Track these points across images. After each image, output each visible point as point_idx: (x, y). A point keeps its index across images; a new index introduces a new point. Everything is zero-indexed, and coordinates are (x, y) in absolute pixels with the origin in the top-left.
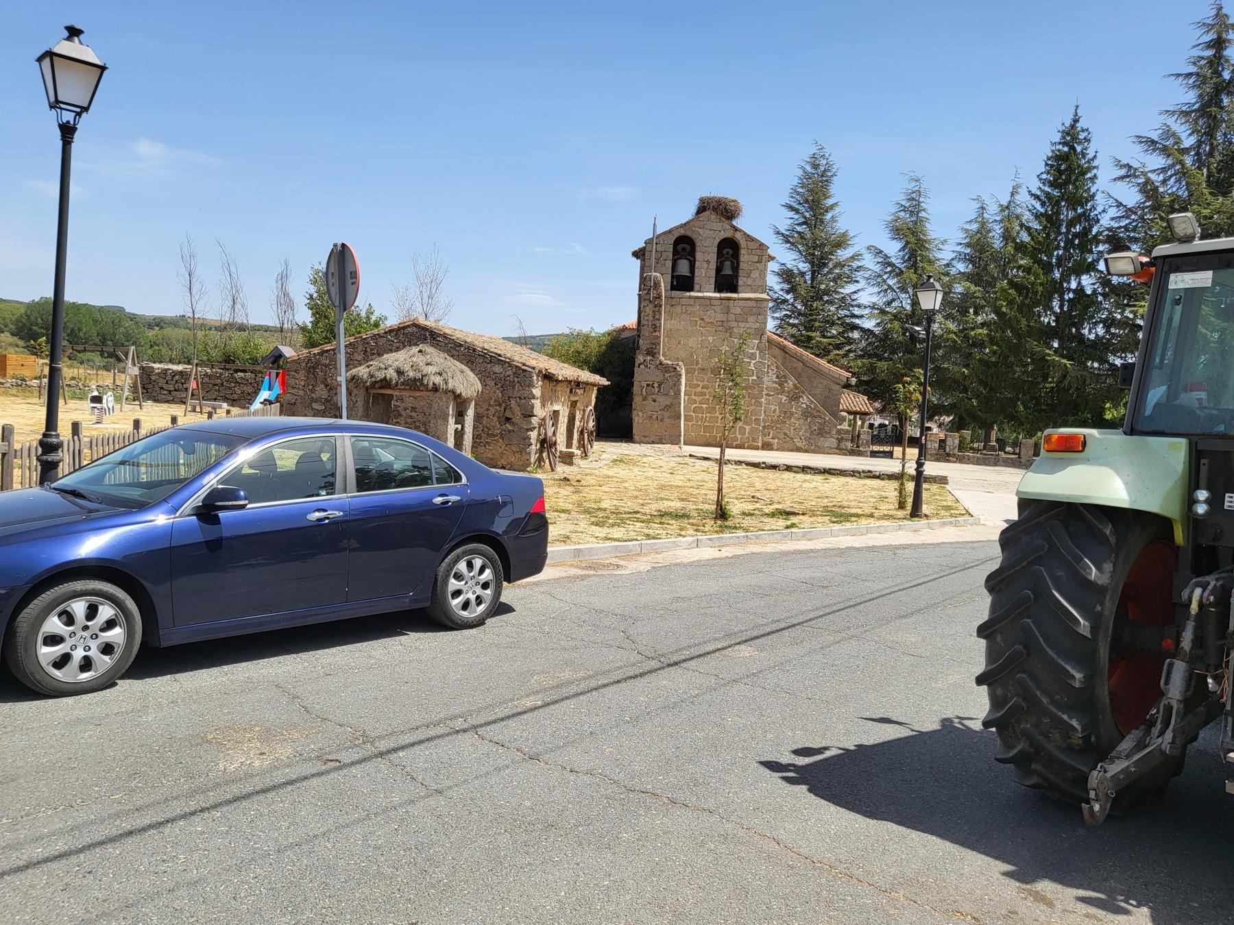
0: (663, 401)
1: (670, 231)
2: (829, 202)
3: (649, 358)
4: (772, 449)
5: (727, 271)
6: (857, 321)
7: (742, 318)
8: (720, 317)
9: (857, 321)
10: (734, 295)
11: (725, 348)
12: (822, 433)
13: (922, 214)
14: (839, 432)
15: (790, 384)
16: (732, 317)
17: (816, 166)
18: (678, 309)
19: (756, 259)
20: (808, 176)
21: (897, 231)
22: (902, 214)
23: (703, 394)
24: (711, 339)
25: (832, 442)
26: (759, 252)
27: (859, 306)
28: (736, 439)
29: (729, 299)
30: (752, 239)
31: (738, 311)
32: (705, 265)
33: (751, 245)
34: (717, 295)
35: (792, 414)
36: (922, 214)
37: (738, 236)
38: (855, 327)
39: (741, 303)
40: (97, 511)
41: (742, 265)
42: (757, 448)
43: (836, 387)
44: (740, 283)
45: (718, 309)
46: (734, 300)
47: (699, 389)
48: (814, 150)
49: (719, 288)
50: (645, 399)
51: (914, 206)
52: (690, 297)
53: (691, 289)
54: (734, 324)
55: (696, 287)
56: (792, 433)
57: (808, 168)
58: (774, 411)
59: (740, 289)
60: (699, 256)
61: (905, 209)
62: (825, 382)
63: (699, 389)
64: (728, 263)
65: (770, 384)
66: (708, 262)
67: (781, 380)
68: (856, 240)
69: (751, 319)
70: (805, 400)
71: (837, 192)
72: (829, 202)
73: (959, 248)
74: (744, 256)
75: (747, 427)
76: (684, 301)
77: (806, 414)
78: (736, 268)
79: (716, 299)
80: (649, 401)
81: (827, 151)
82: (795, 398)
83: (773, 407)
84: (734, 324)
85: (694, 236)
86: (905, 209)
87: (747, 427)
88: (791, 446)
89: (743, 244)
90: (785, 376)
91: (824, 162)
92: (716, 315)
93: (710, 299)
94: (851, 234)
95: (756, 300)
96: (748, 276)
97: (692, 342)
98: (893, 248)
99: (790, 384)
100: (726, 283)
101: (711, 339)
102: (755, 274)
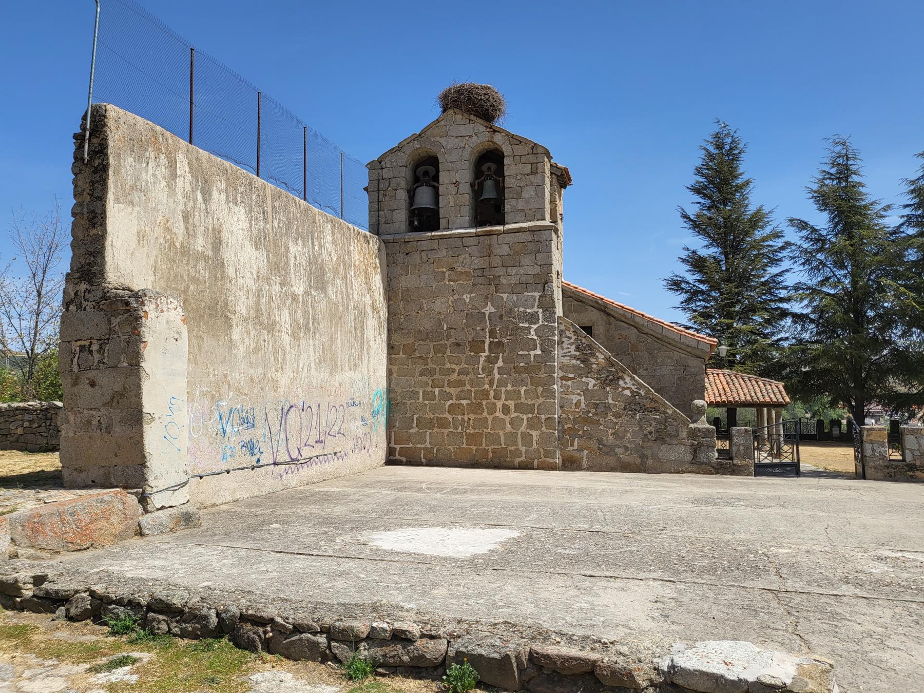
0: (108, 382)
1: (399, 148)
2: (739, 181)
3: (83, 286)
4: (579, 468)
5: (489, 193)
6: (785, 306)
7: (512, 261)
8: (478, 262)
9: (785, 306)
10: (500, 228)
11: (489, 309)
12: (661, 437)
13: (854, 178)
14: (693, 433)
15: (601, 357)
16: (496, 261)
17: (719, 147)
18: (416, 258)
19: (528, 169)
20: (710, 156)
21: (823, 200)
22: (827, 182)
23: (460, 383)
24: (467, 298)
25: (682, 452)
26: (532, 158)
27: (785, 288)
28: (517, 453)
29: (489, 234)
30: (519, 141)
31: (505, 250)
32: (452, 189)
33: (520, 150)
34: (473, 231)
35: (608, 407)
36: (854, 178)
37: (498, 139)
38: (784, 314)
39: (509, 238)
40: (354, 494)
41: (509, 182)
42: (553, 468)
43: (694, 363)
44: (507, 207)
45: (474, 250)
46: (498, 234)
47: (454, 377)
48: (716, 129)
49: (478, 221)
50: (75, 383)
51: (843, 171)
52: (432, 239)
53: (437, 228)
54: (500, 271)
55: (443, 223)
56: (610, 439)
57: (712, 149)
58: (578, 404)
59: (507, 218)
60: (443, 177)
61: (831, 177)
62: (676, 355)
63: (454, 377)
64: (489, 184)
65: (566, 360)
66: (456, 184)
67: (585, 354)
68: (771, 217)
69: (526, 260)
70: (628, 383)
71: (746, 168)
72: (739, 181)
73: (907, 211)
74: (510, 167)
75: (535, 434)
76: (425, 245)
77: (633, 405)
78: (500, 189)
79: (470, 236)
80: (84, 386)
81: (732, 128)
82: (610, 379)
83: (575, 398)
84: (500, 271)
85: (434, 150)
86: (831, 177)
87: (535, 434)
88: (611, 460)
89: (506, 149)
90: (590, 347)
91: (729, 140)
92: (471, 261)
93: (461, 237)
94: (766, 210)
95: (531, 230)
96: (518, 196)
97: (439, 305)
98: (821, 221)
99: (601, 357)
100: (489, 210)
101: (467, 298)
102: (528, 192)
